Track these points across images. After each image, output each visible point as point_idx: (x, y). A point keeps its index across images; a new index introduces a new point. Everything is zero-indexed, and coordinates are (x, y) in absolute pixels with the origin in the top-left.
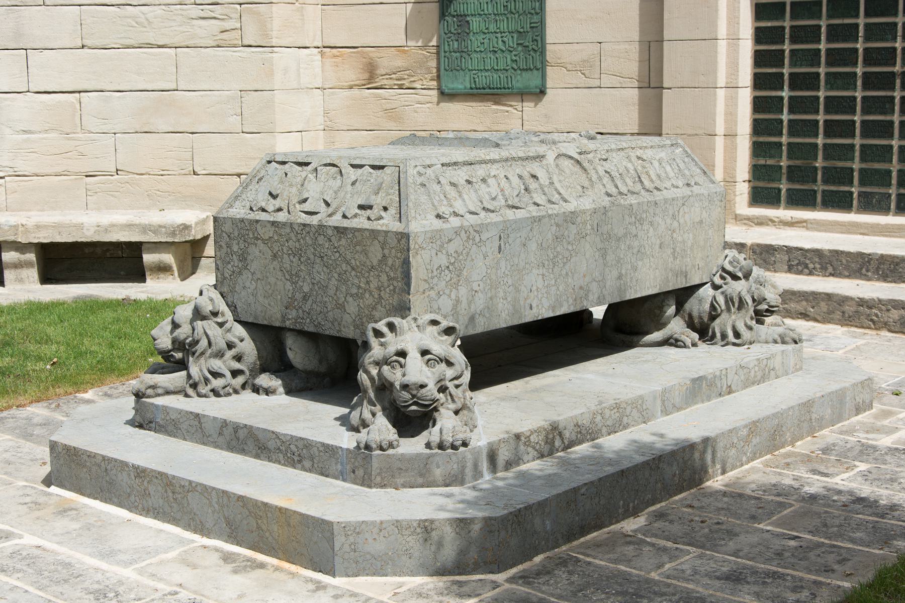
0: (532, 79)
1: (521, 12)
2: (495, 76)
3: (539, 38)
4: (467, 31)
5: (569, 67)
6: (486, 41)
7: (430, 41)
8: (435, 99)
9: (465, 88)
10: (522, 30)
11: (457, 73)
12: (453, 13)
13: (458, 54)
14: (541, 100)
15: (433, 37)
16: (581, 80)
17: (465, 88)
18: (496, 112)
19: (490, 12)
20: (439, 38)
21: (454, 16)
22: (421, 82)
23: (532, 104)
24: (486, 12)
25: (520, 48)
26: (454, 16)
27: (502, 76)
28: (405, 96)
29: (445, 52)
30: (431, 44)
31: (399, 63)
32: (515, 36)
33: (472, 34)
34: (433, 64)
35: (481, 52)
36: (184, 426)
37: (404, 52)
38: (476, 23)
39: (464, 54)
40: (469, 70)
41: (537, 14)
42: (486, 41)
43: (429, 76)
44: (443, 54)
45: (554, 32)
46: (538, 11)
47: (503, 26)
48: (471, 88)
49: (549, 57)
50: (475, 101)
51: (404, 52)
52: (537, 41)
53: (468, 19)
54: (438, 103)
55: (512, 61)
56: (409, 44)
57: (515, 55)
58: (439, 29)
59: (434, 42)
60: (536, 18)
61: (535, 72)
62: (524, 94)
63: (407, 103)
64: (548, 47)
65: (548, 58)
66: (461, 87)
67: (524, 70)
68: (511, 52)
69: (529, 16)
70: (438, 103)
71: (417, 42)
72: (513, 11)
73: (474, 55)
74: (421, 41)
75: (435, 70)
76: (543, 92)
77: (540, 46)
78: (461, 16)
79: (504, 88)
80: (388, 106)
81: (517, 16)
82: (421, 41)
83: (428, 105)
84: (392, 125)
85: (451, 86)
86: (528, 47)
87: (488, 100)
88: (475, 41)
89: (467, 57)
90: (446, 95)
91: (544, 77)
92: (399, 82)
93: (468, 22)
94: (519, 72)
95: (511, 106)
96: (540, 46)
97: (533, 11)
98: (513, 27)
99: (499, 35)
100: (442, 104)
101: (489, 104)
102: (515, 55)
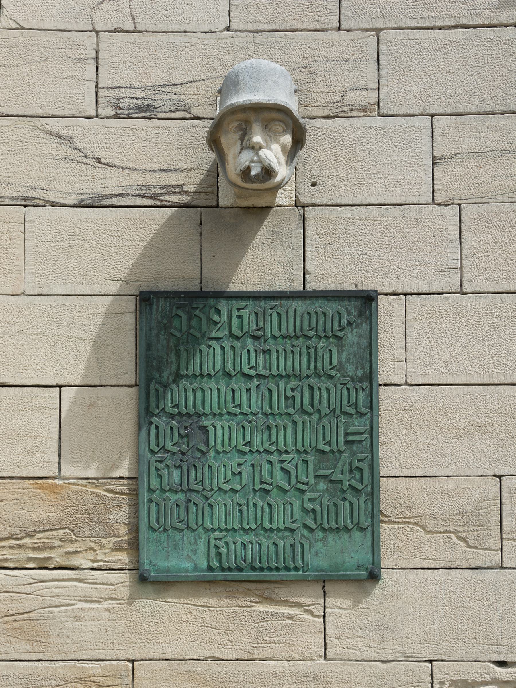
0: (351, 551)
1: (325, 410)
2: (265, 543)
3: (365, 466)
4: (204, 448)
5: (431, 524)
6: (246, 469)
7: (115, 466)
8: (124, 592)
9: (196, 568)
10: (327, 448)
11: (178, 536)
12: (169, 408)
13: (181, 496)
14: (367, 594)
15: (121, 457)
16: (459, 554)
17: (196, 568)
18: (266, 617)
19: (255, 408)
20: (138, 459)
21: (172, 416)
22: (90, 555)
23: (347, 602)
24: (246, 409)
25: (322, 486)
26: (172, 416)
27: (281, 543)
28: (56, 585)
29: (151, 490)
30: (117, 474)
31: (40, 512)
32: (312, 459)
33: (212, 453)
34: (121, 515)
35: (233, 491)
36: (150, 353)
37: (55, 489)
38: (221, 431)
39: (194, 497)
40: (206, 530)
41: (362, 415)
42: (246, 469)
43: (109, 542)
44: (145, 495)
45: (395, 453)
46: (364, 410)
47: (286, 438)
48: (210, 569)
49: (386, 503)
50: (217, 595)
51: (55, 489)
52: (361, 470)
53: (205, 422)
54: (131, 600)
55: (305, 511)
56: (67, 471)
57: (311, 500)
58: (138, 443)
59: (124, 470)
60: (358, 424)
61: (357, 535)
62: (326, 581)
63: (57, 601)
64: (384, 483)
65: (383, 507)
66: (186, 565)
67: (331, 529)
68: (303, 492)
69: (343, 419)
70: (131, 600)
71: (87, 467)
72: (307, 407)
73: (218, 499)
74: (94, 465)
75: (123, 530)
76: (374, 576)
77: (367, 479)
78: (189, 415)
79: (270, 569)
80: (14, 607)
81: (315, 418)
82: (94, 465)
83: (106, 605)
84: (21, 649)
85: (163, 563)
86: (341, 482)
87: (246, 594)
88: (220, 469)
89: (201, 502)
90: (147, 581)
91: (375, 545)
92: (41, 555)
93: (204, 429)
94: (320, 535)
95: (299, 605)
96: (367, 479)
97: (352, 410)
98: (306, 439)
99: (275, 458)
100: (140, 603)
101: (249, 600)
102: (311, 500)
